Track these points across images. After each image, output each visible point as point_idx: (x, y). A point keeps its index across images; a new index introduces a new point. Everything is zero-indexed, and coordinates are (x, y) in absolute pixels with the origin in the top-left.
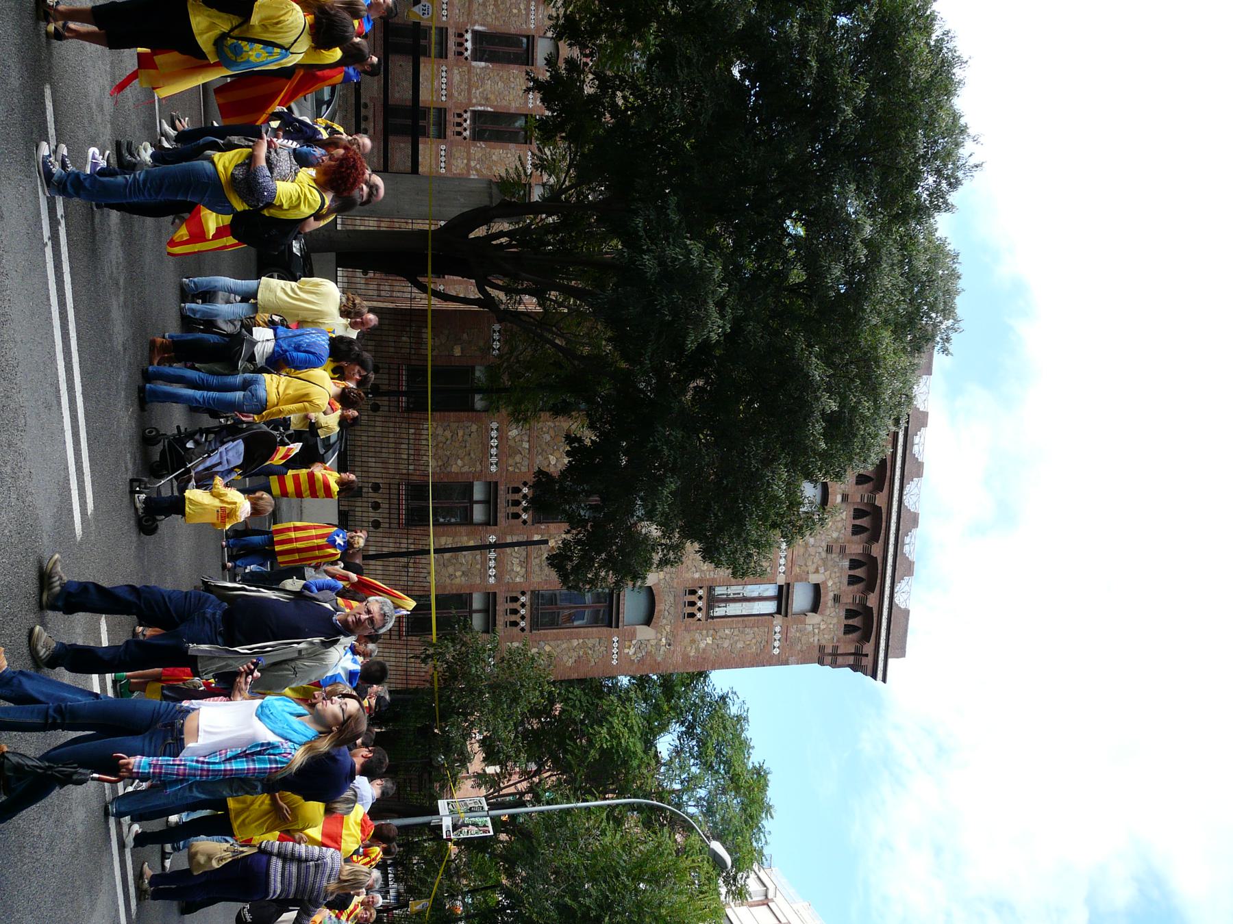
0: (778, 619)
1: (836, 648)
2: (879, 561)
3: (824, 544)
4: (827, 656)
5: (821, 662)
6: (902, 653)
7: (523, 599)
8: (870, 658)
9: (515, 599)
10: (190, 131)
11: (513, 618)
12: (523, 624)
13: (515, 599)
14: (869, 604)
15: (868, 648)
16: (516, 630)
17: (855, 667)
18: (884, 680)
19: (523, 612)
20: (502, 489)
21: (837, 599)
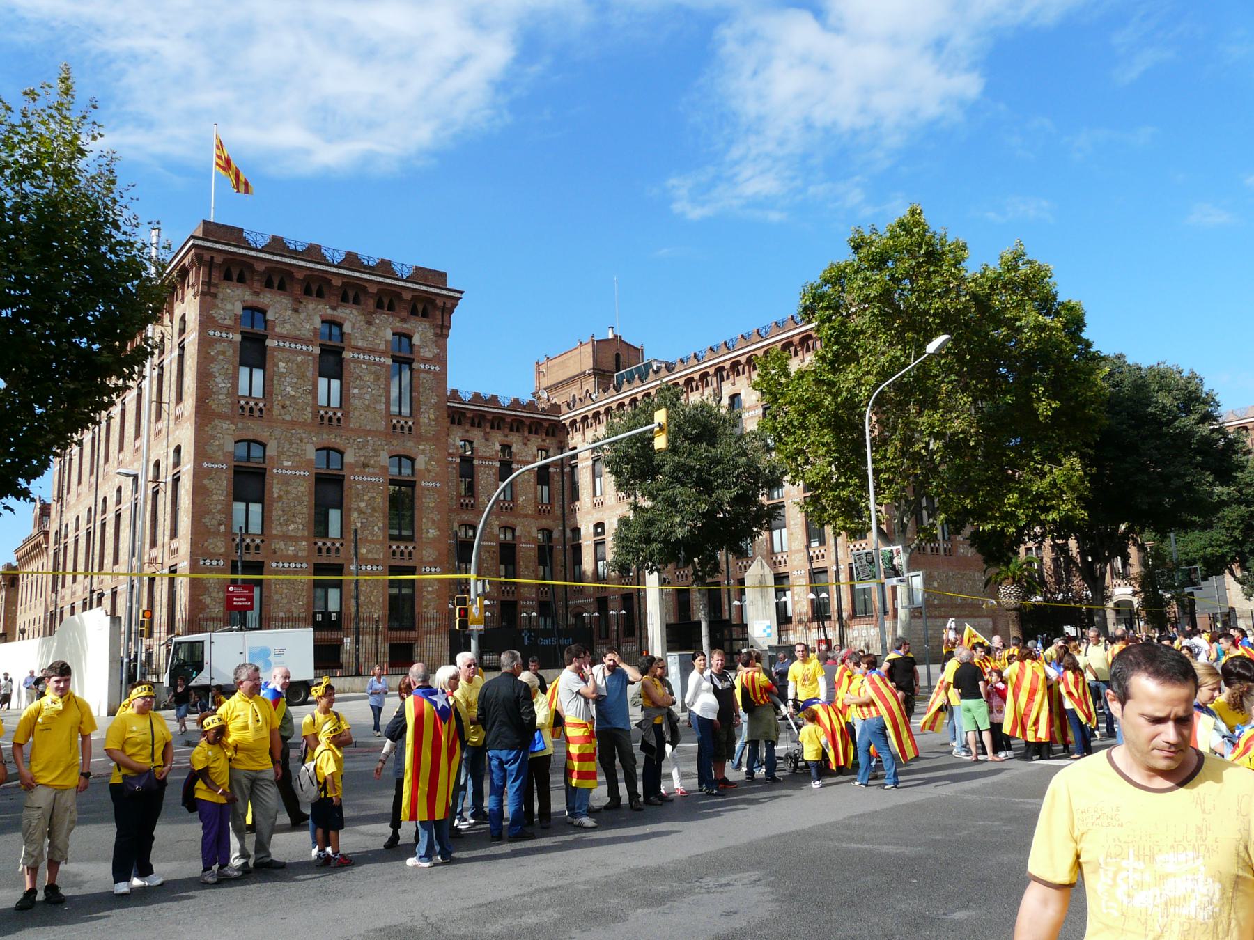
0: (415, 365)
1: (437, 326)
2: (270, 265)
3: (289, 312)
4: (443, 330)
5: (447, 336)
6: (442, 276)
7: (394, 547)
8: (214, 255)
9: (394, 553)
10: (701, 743)
11: (324, 550)
12: (410, 548)
13: (320, 550)
14: (375, 291)
15: (439, 302)
16: (414, 552)
17: (452, 311)
18: (462, 293)
19: (402, 548)
20: (393, 563)
21: (403, 321)
